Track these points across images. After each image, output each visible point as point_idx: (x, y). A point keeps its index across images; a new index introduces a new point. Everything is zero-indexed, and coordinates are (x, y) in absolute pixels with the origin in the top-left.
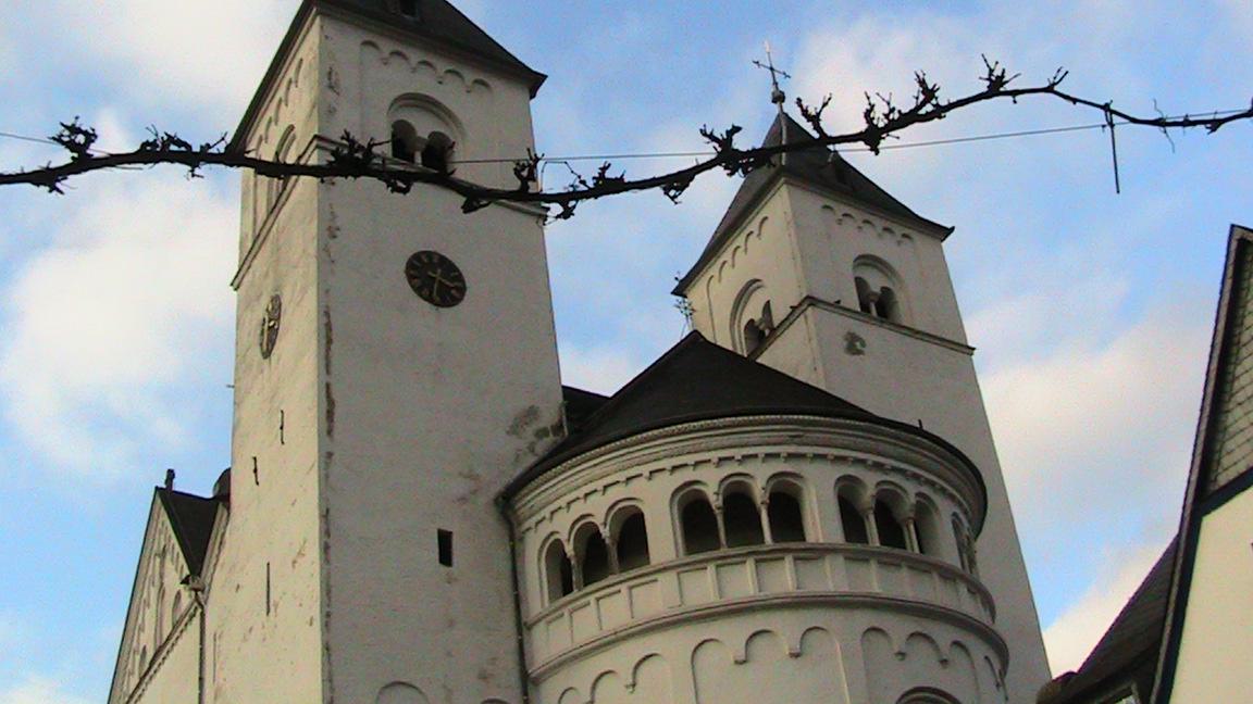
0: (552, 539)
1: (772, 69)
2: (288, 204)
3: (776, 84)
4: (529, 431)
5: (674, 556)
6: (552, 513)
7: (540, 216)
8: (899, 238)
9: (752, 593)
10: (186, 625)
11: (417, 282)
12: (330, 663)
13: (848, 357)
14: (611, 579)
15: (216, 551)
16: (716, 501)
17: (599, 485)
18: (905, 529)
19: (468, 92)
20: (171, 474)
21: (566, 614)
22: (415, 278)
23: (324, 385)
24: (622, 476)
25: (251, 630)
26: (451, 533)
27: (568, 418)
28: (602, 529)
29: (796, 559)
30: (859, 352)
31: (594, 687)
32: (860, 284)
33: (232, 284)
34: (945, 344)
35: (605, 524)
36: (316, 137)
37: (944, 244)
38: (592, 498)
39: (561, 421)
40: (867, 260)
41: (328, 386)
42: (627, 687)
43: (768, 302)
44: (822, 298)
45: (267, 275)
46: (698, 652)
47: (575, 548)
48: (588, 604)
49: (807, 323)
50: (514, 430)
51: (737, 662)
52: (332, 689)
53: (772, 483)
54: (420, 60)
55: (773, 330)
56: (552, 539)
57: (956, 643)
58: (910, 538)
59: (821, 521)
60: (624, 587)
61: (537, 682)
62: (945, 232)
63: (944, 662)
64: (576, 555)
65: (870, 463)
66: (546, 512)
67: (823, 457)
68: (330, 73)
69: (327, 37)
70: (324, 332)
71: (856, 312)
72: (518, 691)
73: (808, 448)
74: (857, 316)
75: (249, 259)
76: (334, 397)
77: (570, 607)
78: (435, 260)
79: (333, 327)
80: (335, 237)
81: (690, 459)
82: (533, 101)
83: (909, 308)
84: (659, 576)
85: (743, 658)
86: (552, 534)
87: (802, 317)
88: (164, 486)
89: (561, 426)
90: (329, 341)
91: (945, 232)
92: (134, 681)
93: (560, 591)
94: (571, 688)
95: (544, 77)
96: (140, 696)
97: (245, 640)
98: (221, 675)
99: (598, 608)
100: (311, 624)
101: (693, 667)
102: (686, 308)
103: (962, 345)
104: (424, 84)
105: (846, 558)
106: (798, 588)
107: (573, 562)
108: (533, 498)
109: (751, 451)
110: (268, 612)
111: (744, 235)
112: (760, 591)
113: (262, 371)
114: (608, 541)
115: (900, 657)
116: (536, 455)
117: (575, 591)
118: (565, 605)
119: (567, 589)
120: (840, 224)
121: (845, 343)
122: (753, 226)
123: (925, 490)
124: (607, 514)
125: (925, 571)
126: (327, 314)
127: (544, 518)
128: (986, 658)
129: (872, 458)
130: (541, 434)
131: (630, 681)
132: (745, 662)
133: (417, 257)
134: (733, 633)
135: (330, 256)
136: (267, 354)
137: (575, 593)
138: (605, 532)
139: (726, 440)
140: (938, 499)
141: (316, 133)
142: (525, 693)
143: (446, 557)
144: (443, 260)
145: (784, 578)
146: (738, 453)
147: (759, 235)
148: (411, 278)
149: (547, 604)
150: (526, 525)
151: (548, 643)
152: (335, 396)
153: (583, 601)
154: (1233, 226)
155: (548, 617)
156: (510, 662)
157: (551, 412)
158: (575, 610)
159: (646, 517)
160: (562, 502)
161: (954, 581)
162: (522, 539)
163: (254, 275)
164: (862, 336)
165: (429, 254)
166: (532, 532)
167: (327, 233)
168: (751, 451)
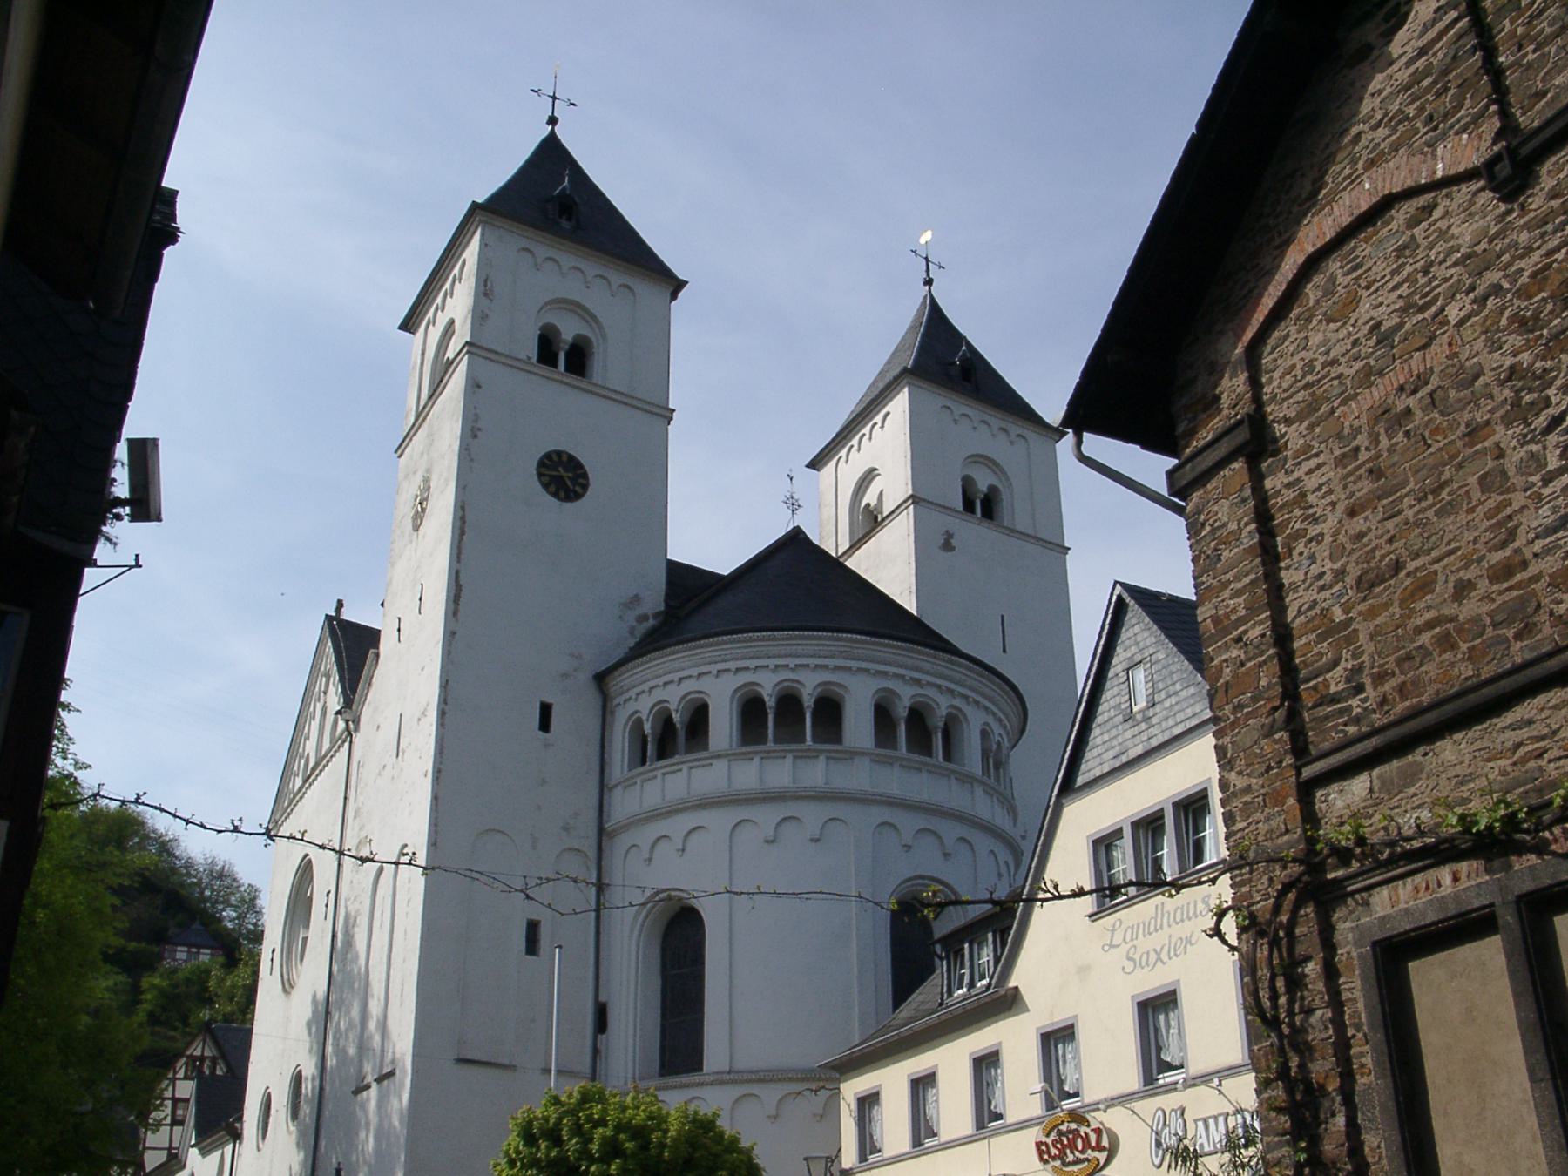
0: (635, 717)
1: (926, 258)
2: (444, 394)
3: (928, 270)
5: (727, 747)
6: (638, 694)
7: (665, 417)
8: (1013, 437)
9: (787, 785)
10: (339, 747)
13: (942, 554)
14: (677, 758)
16: (770, 702)
17: (676, 677)
20: (340, 604)
22: (544, 475)
23: (454, 572)
24: (695, 671)
25: (384, 766)
28: (674, 716)
31: (653, 847)
33: (396, 452)
35: (677, 711)
36: (467, 343)
37: (1058, 445)
38: (669, 687)
41: (457, 572)
42: (645, 860)
45: (422, 454)
46: (739, 828)
47: (652, 728)
48: (655, 777)
51: (767, 841)
52: (436, 832)
53: (819, 690)
54: (571, 265)
55: (883, 520)
56: (635, 717)
59: (858, 725)
60: (685, 767)
61: (613, 834)
62: (678, 285)
63: (946, 855)
64: (653, 733)
65: (907, 678)
66: (632, 693)
67: (867, 671)
68: (486, 281)
69: (486, 245)
70: (458, 523)
71: (957, 511)
73: (853, 662)
74: (960, 516)
75: (412, 433)
78: (565, 458)
80: (476, 436)
81: (752, 663)
82: (673, 303)
83: (1015, 509)
84: (715, 762)
85: (772, 838)
86: (636, 712)
88: (333, 614)
90: (462, 533)
94: (665, 836)
96: (301, 798)
98: (361, 798)
99: (663, 781)
101: (731, 842)
103: (1058, 545)
104: (572, 288)
106: (826, 784)
108: (623, 680)
109: (804, 661)
110: (398, 756)
111: (869, 427)
112: (794, 782)
113: (411, 542)
114: (678, 726)
115: (905, 849)
122: (878, 419)
123: (958, 702)
124: (680, 703)
125: (943, 775)
126: (463, 508)
127: (630, 698)
128: (992, 851)
129: (909, 674)
130: (642, 618)
131: (681, 847)
132: (773, 841)
133: (548, 456)
134: (767, 817)
136: (416, 528)
137: (647, 767)
138: (676, 717)
139: (783, 650)
140: (969, 711)
141: (468, 340)
143: (545, 725)
144: (571, 458)
145: (816, 773)
146: (792, 662)
147: (882, 427)
148: (540, 475)
149: (626, 772)
150: (616, 702)
151: (624, 805)
154: (1116, 582)
155: (627, 784)
157: (654, 598)
158: (645, 781)
159: (710, 708)
160: (646, 687)
161: (972, 784)
162: (612, 713)
163: (413, 449)
165: (559, 453)
166: (621, 707)
167: (470, 433)
168: (804, 661)
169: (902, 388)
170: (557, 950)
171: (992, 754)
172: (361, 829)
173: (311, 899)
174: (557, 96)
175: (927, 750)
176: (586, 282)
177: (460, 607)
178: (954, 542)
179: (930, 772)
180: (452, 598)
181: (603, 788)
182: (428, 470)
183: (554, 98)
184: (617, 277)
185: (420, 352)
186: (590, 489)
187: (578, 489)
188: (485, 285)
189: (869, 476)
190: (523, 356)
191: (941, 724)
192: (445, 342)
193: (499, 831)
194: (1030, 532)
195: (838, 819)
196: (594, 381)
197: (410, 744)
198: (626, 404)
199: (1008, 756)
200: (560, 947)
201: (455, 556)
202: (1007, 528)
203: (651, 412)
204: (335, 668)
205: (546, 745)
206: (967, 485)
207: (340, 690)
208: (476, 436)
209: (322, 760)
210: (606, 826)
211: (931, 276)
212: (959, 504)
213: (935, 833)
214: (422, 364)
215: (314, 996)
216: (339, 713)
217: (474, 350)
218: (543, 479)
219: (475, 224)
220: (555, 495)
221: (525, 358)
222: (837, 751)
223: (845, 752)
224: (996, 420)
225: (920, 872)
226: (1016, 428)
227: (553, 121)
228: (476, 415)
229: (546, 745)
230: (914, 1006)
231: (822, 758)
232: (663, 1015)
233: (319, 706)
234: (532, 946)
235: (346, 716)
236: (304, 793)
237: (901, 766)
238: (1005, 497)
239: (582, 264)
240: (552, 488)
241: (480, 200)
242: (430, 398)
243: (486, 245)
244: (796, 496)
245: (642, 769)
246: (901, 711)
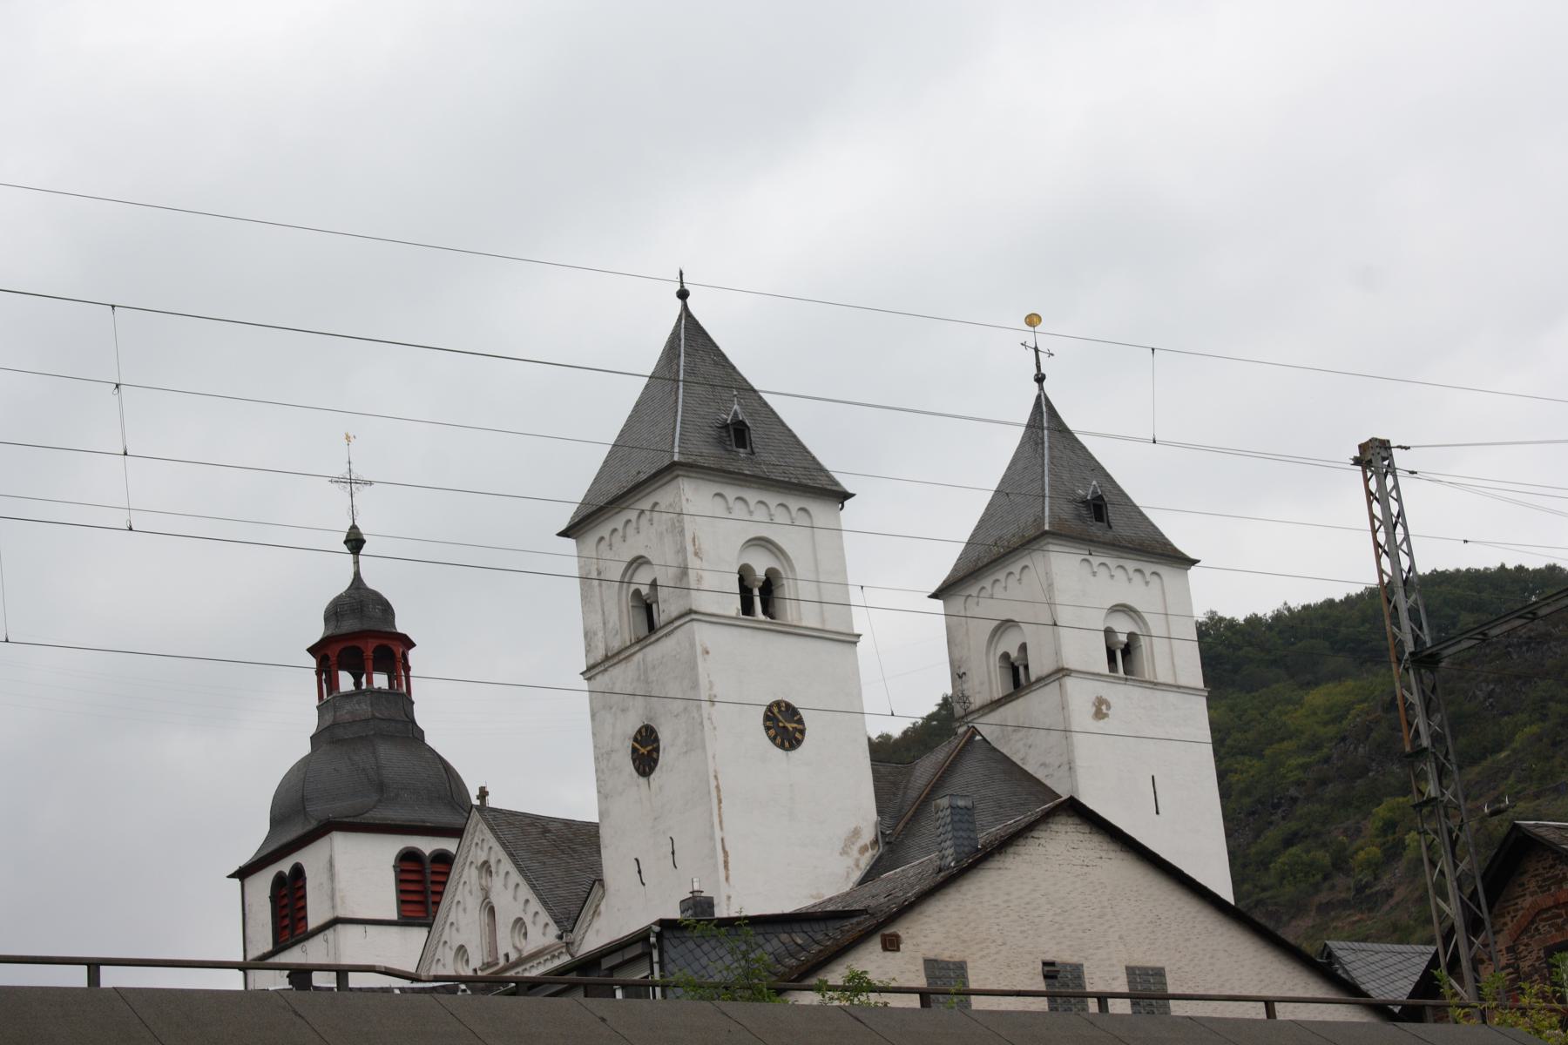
4: (855, 849)
11: (772, 732)
15: (589, 918)
26: (898, 950)
30: (1106, 715)
32: (1109, 633)
34: (1182, 690)
39: (877, 836)
40: (1123, 609)
50: (844, 852)
55: (1030, 684)
79: (721, 788)
89: (877, 840)
116: (861, 869)
120: (1094, 576)
121: (1094, 709)
130: (863, 850)
148: (767, 729)
152: (727, 849)
164: (1109, 699)
177: (730, 872)
211: (1043, 371)
215: (866, 972)
222: (1114, 677)
228: (710, 682)
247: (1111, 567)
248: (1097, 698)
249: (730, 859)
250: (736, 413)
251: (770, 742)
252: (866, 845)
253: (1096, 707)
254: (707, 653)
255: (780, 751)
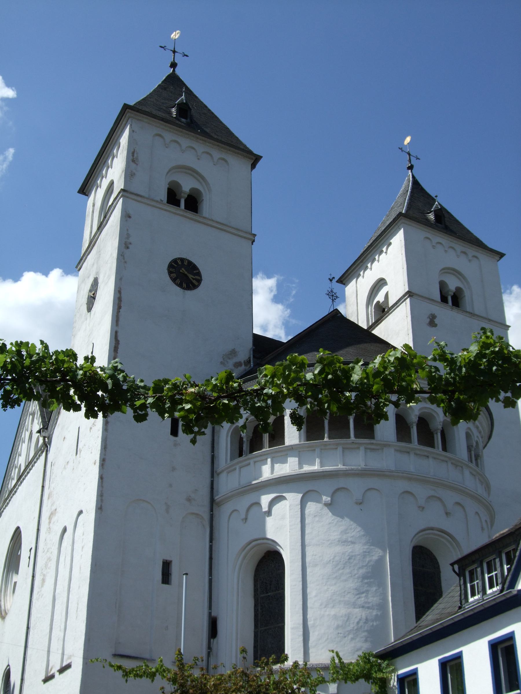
1: (409, 154)
3: (410, 161)
11: (174, 275)
12: (102, 487)
18: (435, 435)
19: (215, 165)
21: (237, 469)
27: (254, 357)
29: (366, 448)
31: (248, 510)
33: (77, 267)
39: (250, 358)
41: (116, 332)
42: (243, 520)
43: (388, 292)
44: (417, 292)
45: (93, 264)
48: (249, 464)
49: (406, 306)
52: (102, 501)
55: (390, 309)
57: (458, 504)
58: (437, 439)
61: (219, 504)
63: (447, 514)
69: (133, 131)
70: (117, 301)
72: (207, 509)
76: (119, 339)
77: (240, 465)
78: (186, 263)
80: (128, 248)
82: (254, 171)
87: (404, 302)
89: (250, 361)
90: (119, 307)
91: (501, 255)
92: (14, 482)
93: (238, 456)
95: (262, 157)
96: (16, 492)
97: (65, 468)
98: (52, 485)
100: (95, 464)
102: (333, 296)
105: (396, 450)
106: (366, 465)
107: (244, 440)
117: (244, 456)
118: (238, 463)
119: (241, 455)
121: (428, 320)
126: (120, 292)
128: (477, 513)
130: (238, 365)
133: (175, 261)
135: (124, 259)
136: (89, 309)
141: (123, 188)
142: (212, 510)
144: (190, 263)
148: (170, 273)
152: (119, 338)
153: (247, 462)
155: (230, 470)
156: (205, 491)
165: (182, 260)
169: (400, 229)
170: (184, 576)
171: (473, 449)
172: (52, 505)
173: (20, 556)
174: (176, 50)
175: (431, 444)
176: (198, 156)
178: (436, 321)
179: (435, 458)
180: (113, 349)
181: (213, 473)
182: (97, 273)
183: (174, 52)
184: (217, 154)
185: (92, 205)
186: (202, 282)
187: (194, 281)
188: (133, 156)
189: (381, 283)
190: (158, 199)
191: (440, 427)
192: (108, 196)
193: (144, 501)
194: (484, 315)
195: (375, 489)
196: (204, 215)
197: (85, 445)
198: (225, 231)
199: (482, 452)
200: (186, 574)
201: (115, 322)
202: (469, 313)
203: (241, 237)
204: (38, 408)
205: (176, 445)
206: (443, 285)
207: (40, 420)
208: (128, 248)
209: (30, 465)
210: (216, 498)
212: (438, 297)
213: (440, 499)
214: (93, 212)
216: (39, 432)
217: (125, 194)
218: (172, 275)
219: (126, 118)
220: (180, 285)
221: (159, 200)
223: (376, 444)
224: (459, 246)
225: (432, 525)
226: (472, 251)
227: (174, 65)
229: (176, 445)
230: (437, 611)
231: (362, 448)
232: (256, 626)
233: (28, 434)
234: (166, 578)
235: (43, 434)
236: (17, 489)
237: (416, 454)
238: (467, 293)
239: (195, 145)
240: (178, 281)
241: (132, 103)
242: (99, 228)
243: (133, 131)
244: (334, 291)
245: (241, 459)
246: (413, 418)
247: (443, 243)
248: (432, 314)
249: (120, 346)
250: (182, 100)
251: (171, 281)
252: (240, 362)
253: (430, 319)
254: (130, 217)
255: (178, 289)
